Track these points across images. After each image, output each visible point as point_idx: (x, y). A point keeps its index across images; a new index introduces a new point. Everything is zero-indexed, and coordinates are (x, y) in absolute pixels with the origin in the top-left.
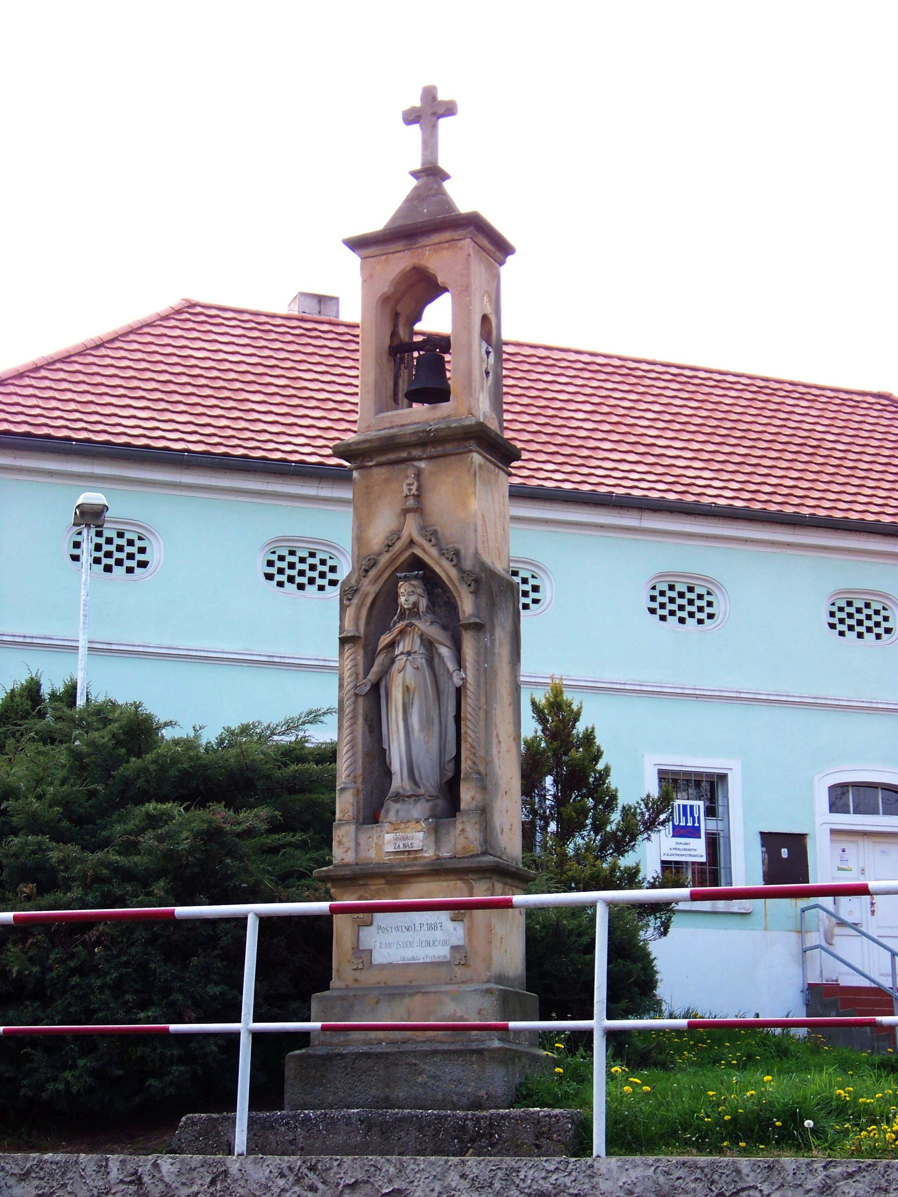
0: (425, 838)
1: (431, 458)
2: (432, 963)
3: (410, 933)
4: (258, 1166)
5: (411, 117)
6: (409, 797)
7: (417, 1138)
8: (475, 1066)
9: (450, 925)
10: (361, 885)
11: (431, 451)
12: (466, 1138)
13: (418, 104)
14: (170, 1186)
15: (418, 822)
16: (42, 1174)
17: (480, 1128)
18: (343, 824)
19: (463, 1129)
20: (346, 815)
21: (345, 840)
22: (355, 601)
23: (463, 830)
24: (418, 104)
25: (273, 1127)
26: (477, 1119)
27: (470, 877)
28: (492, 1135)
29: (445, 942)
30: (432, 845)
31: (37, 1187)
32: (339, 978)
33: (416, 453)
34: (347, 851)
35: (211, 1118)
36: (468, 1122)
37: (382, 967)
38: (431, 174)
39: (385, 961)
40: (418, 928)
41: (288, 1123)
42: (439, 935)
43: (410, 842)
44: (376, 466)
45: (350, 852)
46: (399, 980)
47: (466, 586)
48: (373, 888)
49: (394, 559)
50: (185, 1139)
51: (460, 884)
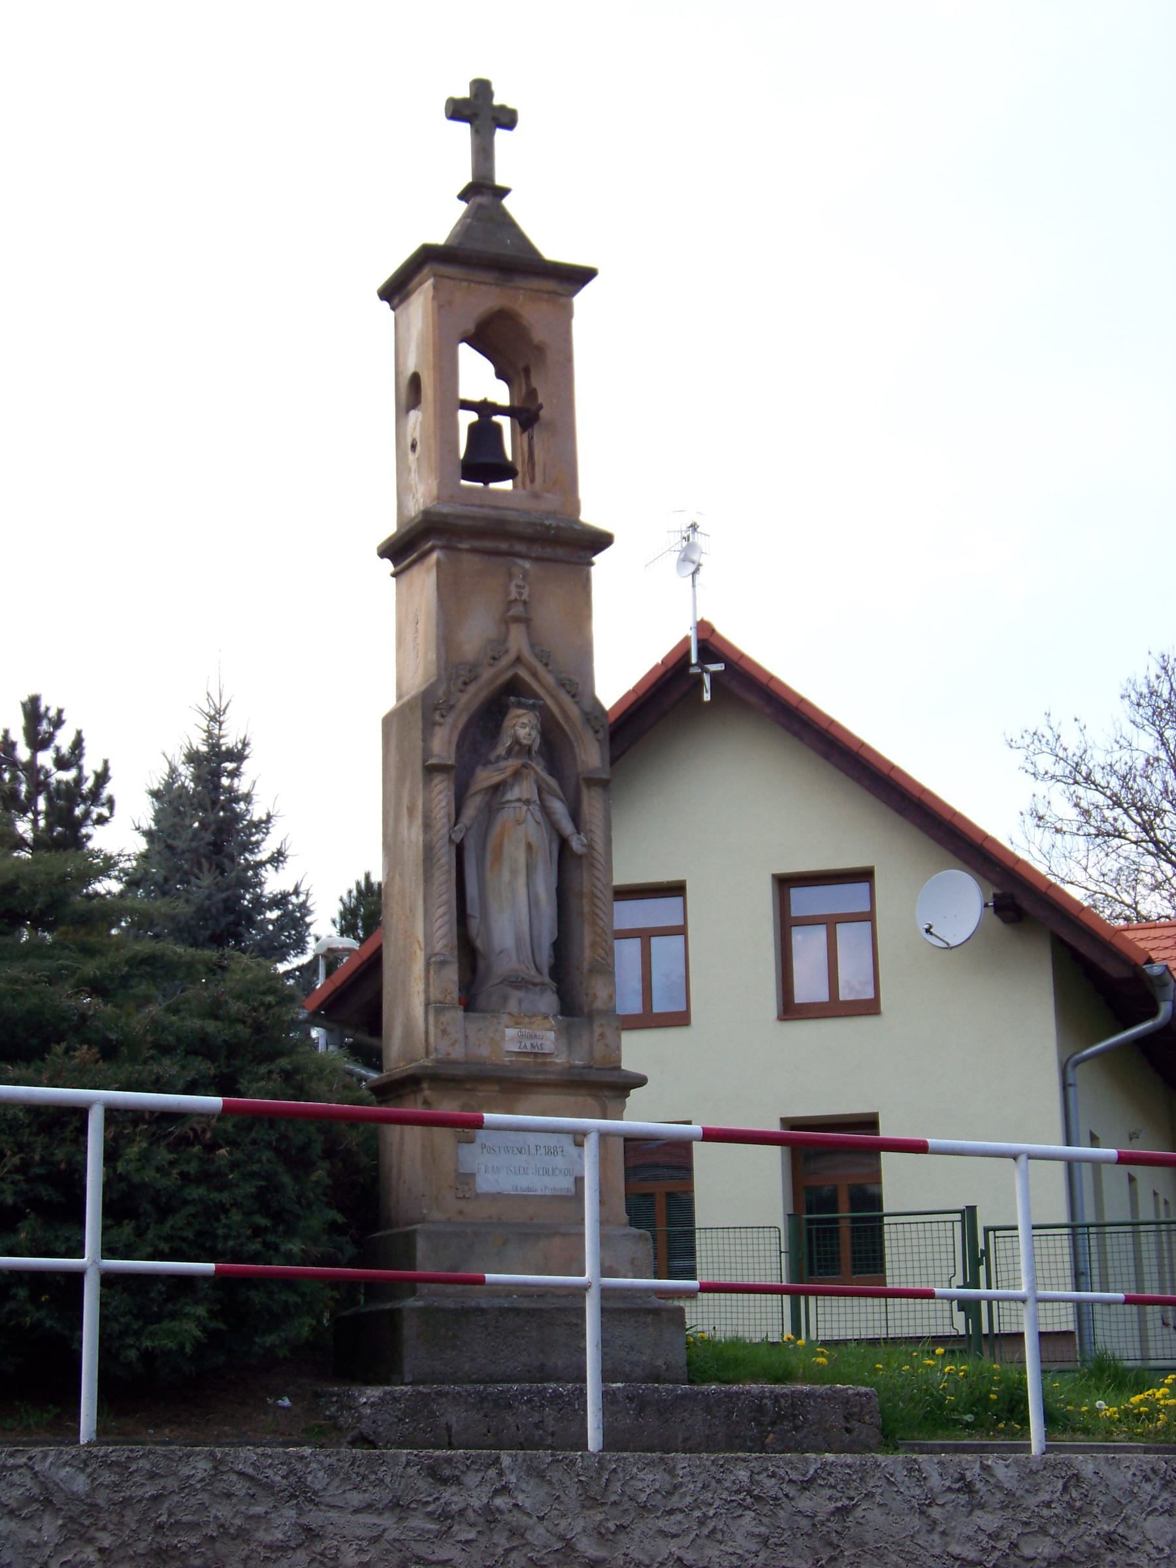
0: (557, 1039)
1: (538, 559)
2: (554, 1197)
3: (525, 1157)
4: (1114, 1468)
5: (457, 111)
6: (535, 985)
7: (704, 1420)
8: (651, 1329)
11: (537, 550)
12: (766, 1420)
13: (497, 101)
14: (1014, 1495)
15: (546, 1017)
16: (832, 1481)
17: (781, 1409)
18: (448, 1008)
19: (761, 1409)
20: (449, 997)
22: (449, 720)
23: (602, 1035)
24: (497, 101)
25: (510, 1406)
26: (776, 1396)
27: (606, 1093)
28: (795, 1416)
31: (830, 1498)
33: (520, 547)
34: (453, 1045)
35: (419, 1392)
36: (765, 1401)
37: (496, 1197)
38: (484, 192)
40: (533, 1151)
41: (530, 1401)
43: (539, 1042)
44: (467, 550)
45: (457, 1045)
47: (590, 732)
48: (480, 1094)
50: (384, 1421)
51: (590, 1101)
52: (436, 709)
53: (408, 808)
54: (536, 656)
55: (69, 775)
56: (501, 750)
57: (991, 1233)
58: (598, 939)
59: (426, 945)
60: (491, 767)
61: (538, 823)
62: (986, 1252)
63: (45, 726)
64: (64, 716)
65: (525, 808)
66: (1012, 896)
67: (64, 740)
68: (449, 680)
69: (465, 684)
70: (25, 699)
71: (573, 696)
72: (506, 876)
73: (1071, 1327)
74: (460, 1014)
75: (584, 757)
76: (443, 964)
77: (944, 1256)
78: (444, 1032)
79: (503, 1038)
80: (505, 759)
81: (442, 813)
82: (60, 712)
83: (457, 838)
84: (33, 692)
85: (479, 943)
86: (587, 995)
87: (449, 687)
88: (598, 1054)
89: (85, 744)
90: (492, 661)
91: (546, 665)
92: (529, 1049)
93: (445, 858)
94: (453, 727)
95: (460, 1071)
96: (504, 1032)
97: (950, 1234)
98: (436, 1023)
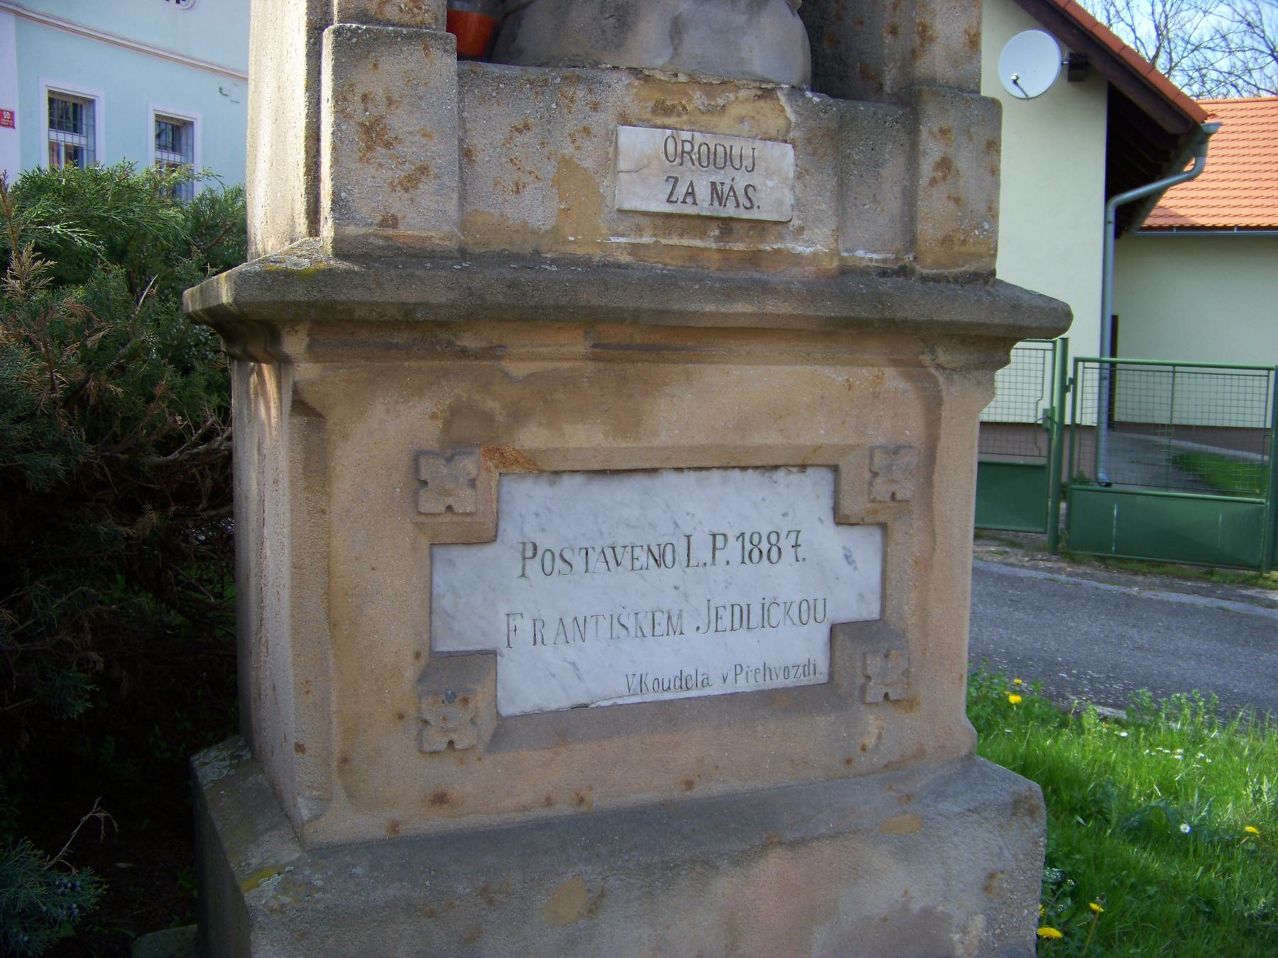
3: (670, 575)
9: (829, 540)
10: (463, 353)
15: (767, 94)
21: (401, 122)
23: (945, 165)
27: (943, 358)
29: (807, 611)
30: (825, 206)
32: (351, 795)
34: (410, 183)
39: (559, 701)
40: (702, 553)
42: (784, 580)
45: (427, 185)
46: (637, 779)
48: (519, 369)
51: (893, 380)
57: (1080, 364)
62: (1074, 381)
79: (610, 163)
88: (928, 231)
92: (704, 206)
95: (433, 291)
96: (612, 138)
97: (1040, 361)
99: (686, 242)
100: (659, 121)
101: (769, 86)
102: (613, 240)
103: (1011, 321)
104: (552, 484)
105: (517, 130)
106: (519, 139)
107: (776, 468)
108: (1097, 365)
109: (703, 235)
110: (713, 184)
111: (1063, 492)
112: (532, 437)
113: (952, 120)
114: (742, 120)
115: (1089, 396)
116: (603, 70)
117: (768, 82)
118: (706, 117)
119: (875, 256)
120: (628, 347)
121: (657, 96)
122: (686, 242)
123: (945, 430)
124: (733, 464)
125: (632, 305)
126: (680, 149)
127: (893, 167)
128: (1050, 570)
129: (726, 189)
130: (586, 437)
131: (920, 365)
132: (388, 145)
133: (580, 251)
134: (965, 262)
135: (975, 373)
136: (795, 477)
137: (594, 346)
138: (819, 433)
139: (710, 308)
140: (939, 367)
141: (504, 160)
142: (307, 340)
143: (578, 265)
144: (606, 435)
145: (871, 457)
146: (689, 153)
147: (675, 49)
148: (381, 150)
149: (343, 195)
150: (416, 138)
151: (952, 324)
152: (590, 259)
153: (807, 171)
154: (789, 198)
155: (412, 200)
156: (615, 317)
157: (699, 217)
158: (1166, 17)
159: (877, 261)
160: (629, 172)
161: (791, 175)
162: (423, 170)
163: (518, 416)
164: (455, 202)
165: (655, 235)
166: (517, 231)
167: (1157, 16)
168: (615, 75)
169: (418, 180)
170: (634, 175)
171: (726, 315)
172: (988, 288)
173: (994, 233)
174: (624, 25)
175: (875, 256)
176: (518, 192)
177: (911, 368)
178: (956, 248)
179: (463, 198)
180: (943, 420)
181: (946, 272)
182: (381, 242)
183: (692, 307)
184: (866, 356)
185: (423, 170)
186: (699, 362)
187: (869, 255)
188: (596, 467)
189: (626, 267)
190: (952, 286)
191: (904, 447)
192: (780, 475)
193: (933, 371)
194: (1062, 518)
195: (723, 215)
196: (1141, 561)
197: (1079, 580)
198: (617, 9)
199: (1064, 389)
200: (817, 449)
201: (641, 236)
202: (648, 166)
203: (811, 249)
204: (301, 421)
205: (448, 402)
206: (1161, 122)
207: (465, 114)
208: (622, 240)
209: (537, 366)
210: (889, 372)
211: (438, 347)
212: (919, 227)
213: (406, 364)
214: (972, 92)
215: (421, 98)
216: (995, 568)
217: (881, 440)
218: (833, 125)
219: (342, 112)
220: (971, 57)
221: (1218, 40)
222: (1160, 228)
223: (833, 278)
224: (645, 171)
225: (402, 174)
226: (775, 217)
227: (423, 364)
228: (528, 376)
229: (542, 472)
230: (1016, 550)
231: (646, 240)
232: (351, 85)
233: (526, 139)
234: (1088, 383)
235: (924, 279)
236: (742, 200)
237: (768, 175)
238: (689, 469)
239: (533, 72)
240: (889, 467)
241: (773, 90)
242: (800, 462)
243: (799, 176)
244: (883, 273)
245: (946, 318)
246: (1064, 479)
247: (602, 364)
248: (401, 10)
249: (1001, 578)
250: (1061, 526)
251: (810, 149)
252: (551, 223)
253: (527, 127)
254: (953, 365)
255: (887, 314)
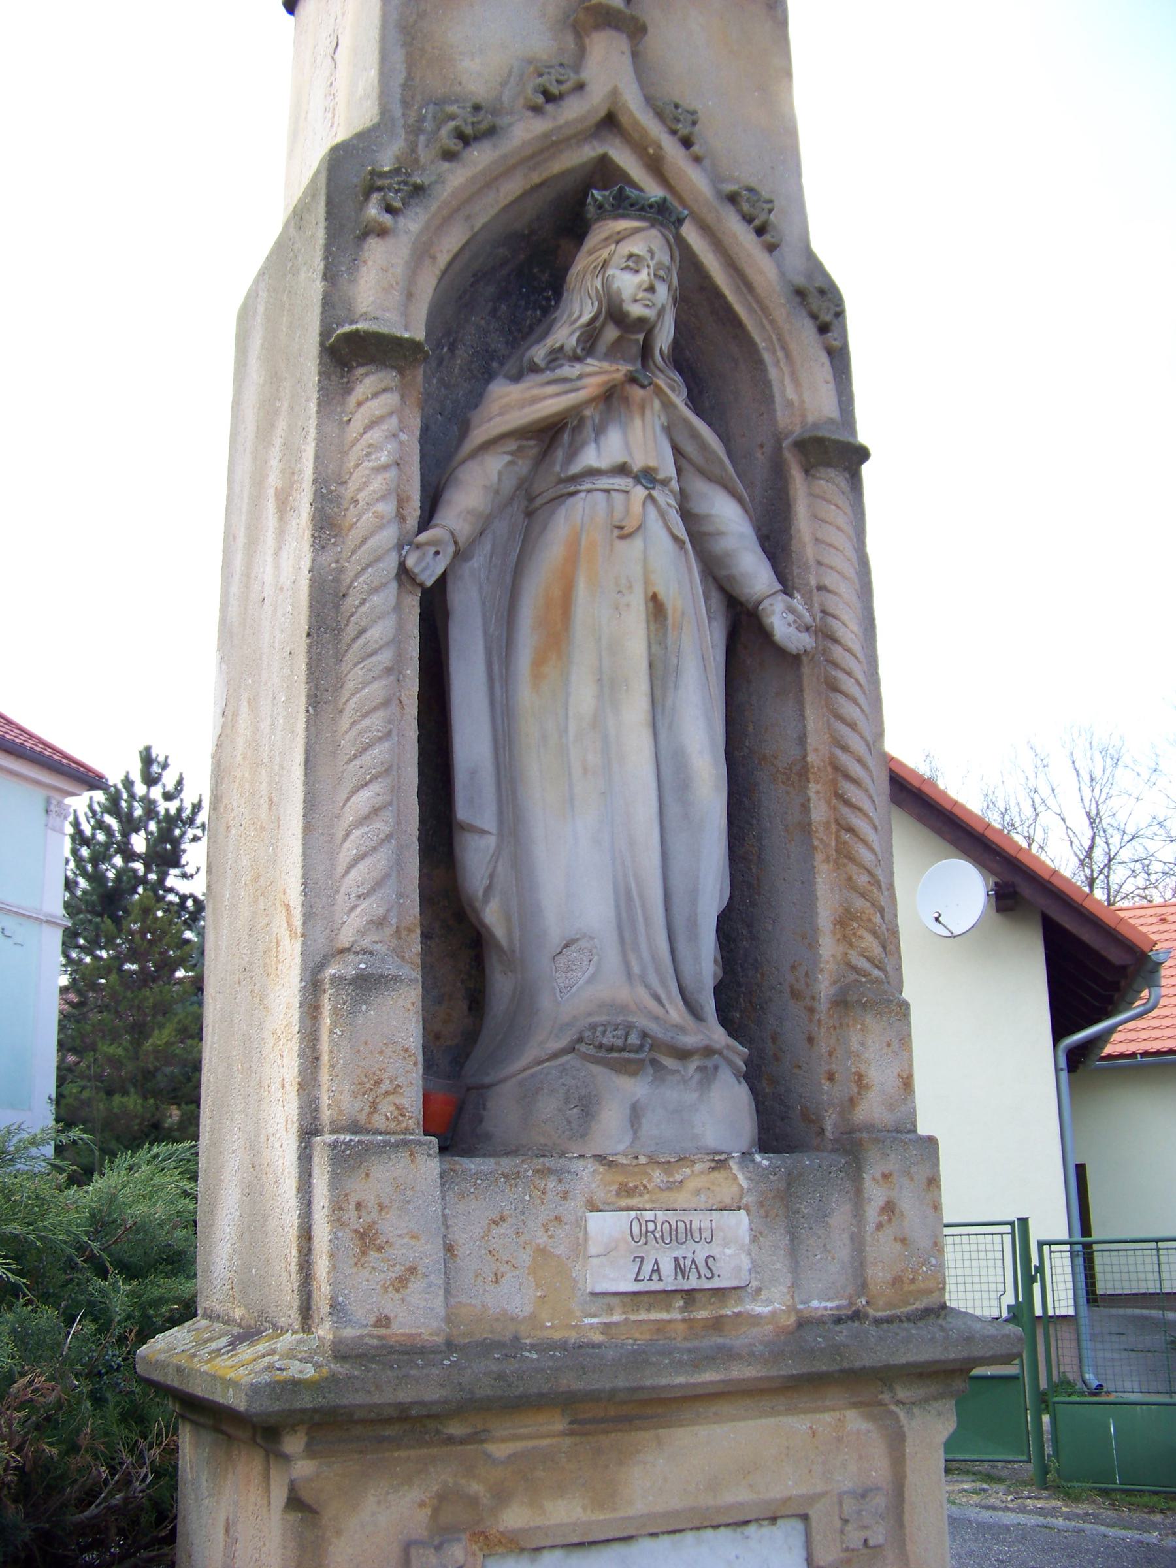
6: (684, 1055)
10: (450, 1440)
15: (720, 1164)
20: (386, 1107)
21: (391, 1226)
22: (412, 224)
23: (889, 1208)
27: (902, 1393)
30: (780, 1264)
34: (401, 1283)
45: (416, 1285)
48: (499, 1450)
49: (554, 144)
51: (855, 1422)
52: (371, 189)
53: (277, 495)
54: (660, 115)
55: (173, 806)
56: (564, 335)
57: (1046, 1248)
58: (859, 903)
59: (308, 916)
60: (532, 380)
61: (676, 539)
62: (1040, 1269)
63: (155, 768)
64: (169, 761)
65: (640, 493)
66: (1013, 885)
67: (169, 781)
68: (415, 130)
69: (465, 139)
70: (141, 748)
71: (760, 231)
72: (583, 695)
73: (1071, 1312)
74: (428, 1166)
75: (790, 393)
76: (366, 985)
77: (992, 1271)
78: (367, 1239)
79: (579, 1247)
80: (577, 359)
81: (378, 483)
82: (167, 758)
83: (429, 571)
84: (147, 744)
85: (492, 915)
86: (831, 1078)
87: (413, 148)
88: (878, 1275)
89: (185, 782)
90: (540, 99)
91: (687, 143)
92: (669, 1281)
93: (385, 627)
94: (422, 253)
95: (426, 1389)
96: (581, 1224)
97: (998, 1247)
98: (337, 1207)
99: (655, 1315)
100: (624, 1202)
101: (722, 1157)
102: (587, 1321)
103: (965, 1354)
104: (533, 1561)
105: (494, 1222)
106: (496, 1231)
107: (746, 1523)
108: (1067, 1247)
109: (668, 1308)
110: (676, 1259)
111: (1043, 1402)
112: (514, 1517)
113: (892, 1163)
114: (698, 1192)
115: (1063, 1295)
116: (570, 1159)
117: (720, 1153)
118: (666, 1194)
119: (829, 1304)
120: (603, 1421)
121: (621, 1179)
122: (655, 1315)
123: (910, 1466)
124: (705, 1524)
125: (608, 1386)
126: (644, 1229)
127: (840, 1216)
128: (1041, 1512)
129: (688, 1262)
130: (566, 1512)
131: (881, 1404)
132: (380, 1249)
133: (557, 1336)
134: (916, 1300)
135: (936, 1405)
136: (767, 1530)
137: (571, 1423)
138: (788, 1484)
139: (680, 1380)
140: (899, 1403)
141: (483, 1252)
142: (305, 1439)
143: (555, 1350)
144: (584, 1509)
145: (841, 1504)
146: (652, 1232)
147: (635, 1133)
148: (373, 1254)
149: (341, 1299)
150: (405, 1240)
151: (908, 1364)
152: (566, 1342)
153: (761, 1233)
154: (746, 1263)
155: (403, 1300)
156: (593, 1397)
157: (665, 1291)
158: (1097, 803)
159: (831, 1309)
160: (599, 1256)
161: (747, 1240)
162: (412, 1270)
163: (502, 1497)
164: (441, 1298)
165: (624, 1313)
166: (497, 1320)
167: (1087, 804)
168: (581, 1162)
169: (408, 1280)
170: (603, 1259)
171: (694, 1385)
172: (940, 1322)
173: (941, 1266)
174: (587, 1114)
175: (829, 1304)
176: (497, 1281)
177: (871, 1408)
178: (906, 1288)
179: (447, 1292)
180: (907, 1456)
181: (898, 1312)
182: (375, 1342)
183: (664, 1381)
184: (828, 1403)
185: (412, 1270)
186: (670, 1427)
187: (824, 1304)
188: (576, 1540)
189: (599, 1346)
190: (905, 1325)
191: (871, 1490)
192: (751, 1529)
193: (893, 1408)
194: (1047, 1436)
195: (686, 1287)
196: (1156, 1493)
197: (1080, 1524)
198: (580, 1100)
199: (1029, 1280)
200: (787, 1500)
201: (612, 1314)
202: (615, 1249)
203: (769, 1308)
204: (294, 1517)
205: (435, 1489)
206: (1103, 953)
207: (447, 1211)
208: (595, 1320)
209: (519, 1446)
210: (851, 1414)
211: (427, 1437)
212: (869, 1272)
213: (396, 1455)
214: (909, 1132)
215: (408, 1202)
216: (973, 1513)
217: (848, 1485)
218: (782, 1186)
219: (339, 1220)
220: (905, 1099)
221: (1156, 828)
222: (1122, 1056)
223: (792, 1333)
224: (614, 1253)
225: (394, 1275)
226: (735, 1284)
227: (412, 1453)
228: (509, 1456)
229: (522, 1550)
230: (995, 1487)
231: (616, 1318)
232: (346, 1195)
233: (503, 1231)
234: (1058, 1270)
235: (878, 1322)
236: (704, 1271)
237: (726, 1245)
238: (663, 1533)
239: (506, 1164)
240: (859, 1513)
241: (726, 1160)
242: (770, 1515)
243: (754, 1239)
244: (838, 1320)
245: (903, 1360)
246: (1043, 1385)
247: (578, 1438)
248: (388, 1119)
249: (982, 1527)
250: (1048, 1450)
251: (762, 1212)
252: (528, 1309)
253: (503, 1219)
254: (913, 1400)
255: (846, 1365)
